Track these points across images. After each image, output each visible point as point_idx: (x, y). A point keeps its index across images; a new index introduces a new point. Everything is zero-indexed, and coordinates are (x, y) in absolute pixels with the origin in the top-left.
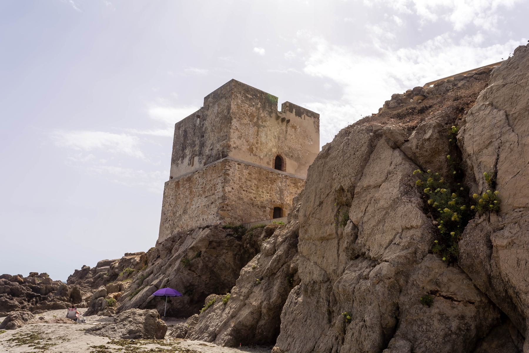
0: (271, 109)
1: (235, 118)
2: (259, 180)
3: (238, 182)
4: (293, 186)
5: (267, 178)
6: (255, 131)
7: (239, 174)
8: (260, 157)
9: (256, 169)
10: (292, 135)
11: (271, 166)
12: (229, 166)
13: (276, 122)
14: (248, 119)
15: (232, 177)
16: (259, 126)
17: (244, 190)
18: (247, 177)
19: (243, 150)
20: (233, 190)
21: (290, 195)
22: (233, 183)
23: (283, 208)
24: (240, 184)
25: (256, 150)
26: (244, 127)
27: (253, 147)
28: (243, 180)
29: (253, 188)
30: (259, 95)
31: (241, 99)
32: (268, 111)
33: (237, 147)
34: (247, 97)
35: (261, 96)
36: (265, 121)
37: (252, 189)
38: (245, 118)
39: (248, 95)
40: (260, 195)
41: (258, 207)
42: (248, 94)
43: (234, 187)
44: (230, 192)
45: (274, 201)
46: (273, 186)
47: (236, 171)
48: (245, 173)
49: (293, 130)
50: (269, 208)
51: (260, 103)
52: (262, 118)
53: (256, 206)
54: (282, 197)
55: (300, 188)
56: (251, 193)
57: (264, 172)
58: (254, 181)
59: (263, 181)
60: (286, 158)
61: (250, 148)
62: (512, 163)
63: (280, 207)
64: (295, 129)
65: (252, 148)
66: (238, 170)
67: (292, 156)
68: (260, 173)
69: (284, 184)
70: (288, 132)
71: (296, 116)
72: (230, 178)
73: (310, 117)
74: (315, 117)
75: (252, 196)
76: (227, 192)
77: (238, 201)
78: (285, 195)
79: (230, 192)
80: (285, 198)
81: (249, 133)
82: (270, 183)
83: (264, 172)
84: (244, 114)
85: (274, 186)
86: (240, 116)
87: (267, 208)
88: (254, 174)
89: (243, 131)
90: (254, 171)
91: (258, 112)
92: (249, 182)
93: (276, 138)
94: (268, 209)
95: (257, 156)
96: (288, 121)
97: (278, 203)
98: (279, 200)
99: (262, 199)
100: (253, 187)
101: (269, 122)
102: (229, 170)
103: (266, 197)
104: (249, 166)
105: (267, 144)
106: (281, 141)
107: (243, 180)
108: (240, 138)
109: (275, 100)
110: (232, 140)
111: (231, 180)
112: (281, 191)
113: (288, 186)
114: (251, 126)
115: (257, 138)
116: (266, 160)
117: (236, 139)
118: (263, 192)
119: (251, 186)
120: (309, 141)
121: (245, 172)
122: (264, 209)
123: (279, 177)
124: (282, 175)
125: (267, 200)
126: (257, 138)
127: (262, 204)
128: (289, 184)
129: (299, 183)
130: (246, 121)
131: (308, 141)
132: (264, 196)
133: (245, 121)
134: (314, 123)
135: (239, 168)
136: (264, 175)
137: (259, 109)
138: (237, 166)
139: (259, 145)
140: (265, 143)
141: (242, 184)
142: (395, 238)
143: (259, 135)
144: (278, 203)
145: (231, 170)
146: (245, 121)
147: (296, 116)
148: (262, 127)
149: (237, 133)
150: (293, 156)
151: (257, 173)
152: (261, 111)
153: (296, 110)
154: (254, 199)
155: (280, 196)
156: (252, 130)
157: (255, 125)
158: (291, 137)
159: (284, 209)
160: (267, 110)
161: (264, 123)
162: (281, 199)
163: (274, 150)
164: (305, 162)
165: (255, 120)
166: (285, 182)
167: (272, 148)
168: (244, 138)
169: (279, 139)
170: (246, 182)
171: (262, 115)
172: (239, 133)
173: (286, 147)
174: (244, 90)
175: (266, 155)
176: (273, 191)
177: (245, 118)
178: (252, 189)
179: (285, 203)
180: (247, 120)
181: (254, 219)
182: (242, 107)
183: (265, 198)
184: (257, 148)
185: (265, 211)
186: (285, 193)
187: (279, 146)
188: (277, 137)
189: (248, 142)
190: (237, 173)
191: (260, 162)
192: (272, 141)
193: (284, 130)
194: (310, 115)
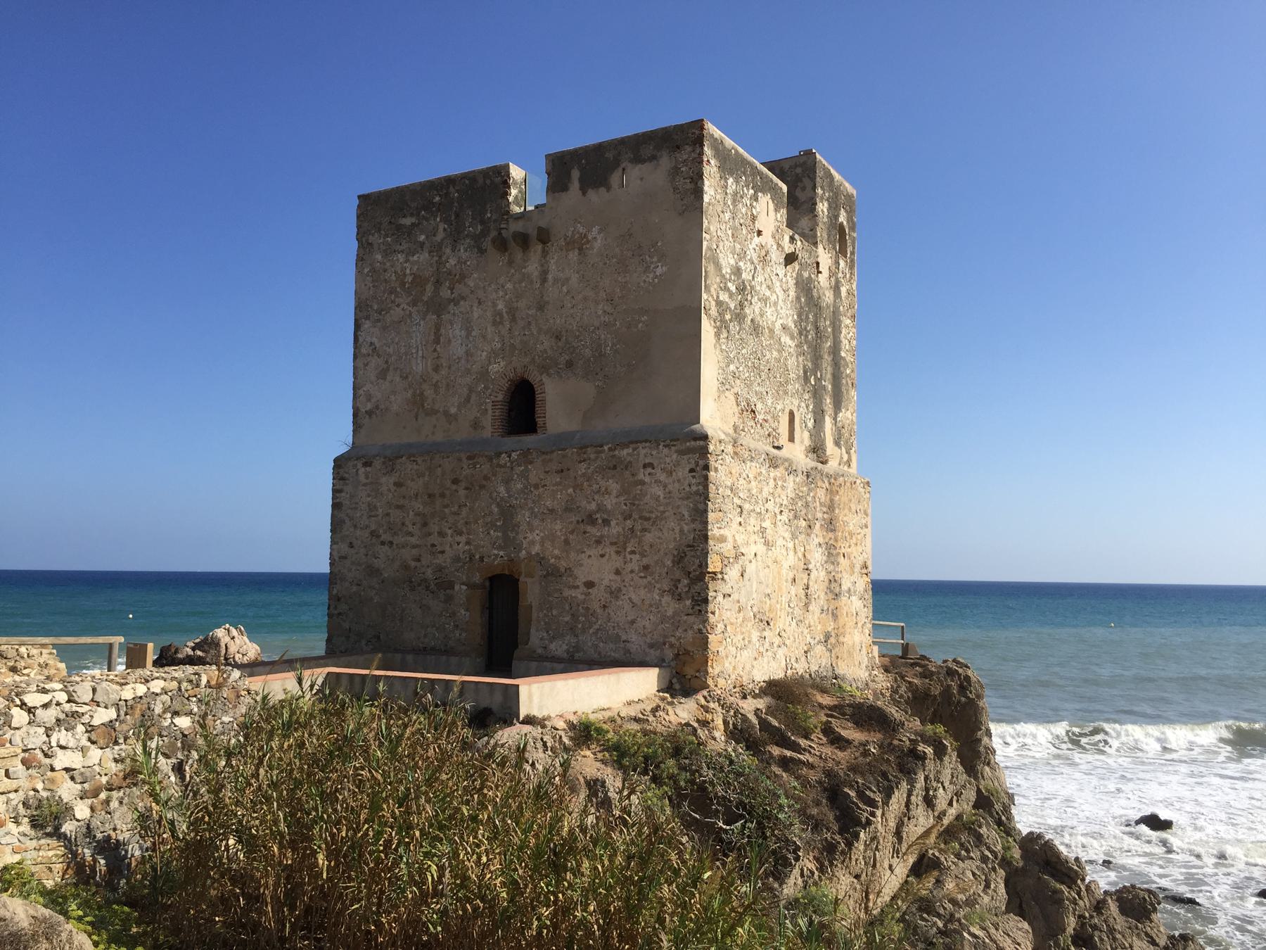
0: (482, 222)
1: (367, 318)
4: (557, 484)
8: (446, 413)
10: (568, 280)
11: (489, 426)
12: (343, 479)
15: (349, 511)
17: (383, 543)
20: (353, 551)
22: (352, 529)
23: (520, 574)
27: (425, 386)
28: (380, 510)
29: (411, 529)
30: (437, 199)
31: (383, 247)
33: (377, 407)
40: (433, 545)
41: (427, 588)
42: (404, 216)
44: (345, 558)
45: (482, 559)
47: (360, 488)
48: (384, 488)
50: (463, 584)
51: (442, 226)
52: (450, 273)
54: (511, 535)
56: (403, 547)
60: (545, 378)
61: (414, 395)
64: (580, 249)
66: (365, 485)
67: (570, 364)
69: (519, 486)
70: (550, 277)
71: (584, 193)
73: (653, 158)
76: (337, 559)
78: (524, 527)
81: (410, 347)
87: (457, 587)
89: (391, 350)
91: (436, 258)
94: (460, 589)
97: (494, 560)
98: (500, 548)
99: (439, 560)
100: (410, 526)
104: (397, 458)
107: (380, 510)
108: (382, 374)
111: (347, 521)
117: (372, 383)
119: (403, 524)
121: (387, 482)
124: (509, 456)
125: (457, 559)
126: (435, 350)
129: (583, 466)
130: (398, 310)
132: (447, 548)
133: (397, 313)
134: (675, 171)
138: (362, 470)
143: (442, 340)
144: (497, 557)
147: (584, 193)
149: (374, 361)
152: (448, 251)
154: (413, 564)
159: (522, 579)
161: (459, 288)
167: (490, 363)
168: (396, 369)
169: (513, 320)
171: (452, 262)
175: (468, 400)
180: (402, 306)
181: (412, 630)
184: (436, 386)
185: (449, 599)
186: (523, 517)
189: (407, 377)
192: (489, 336)
194: (647, 151)
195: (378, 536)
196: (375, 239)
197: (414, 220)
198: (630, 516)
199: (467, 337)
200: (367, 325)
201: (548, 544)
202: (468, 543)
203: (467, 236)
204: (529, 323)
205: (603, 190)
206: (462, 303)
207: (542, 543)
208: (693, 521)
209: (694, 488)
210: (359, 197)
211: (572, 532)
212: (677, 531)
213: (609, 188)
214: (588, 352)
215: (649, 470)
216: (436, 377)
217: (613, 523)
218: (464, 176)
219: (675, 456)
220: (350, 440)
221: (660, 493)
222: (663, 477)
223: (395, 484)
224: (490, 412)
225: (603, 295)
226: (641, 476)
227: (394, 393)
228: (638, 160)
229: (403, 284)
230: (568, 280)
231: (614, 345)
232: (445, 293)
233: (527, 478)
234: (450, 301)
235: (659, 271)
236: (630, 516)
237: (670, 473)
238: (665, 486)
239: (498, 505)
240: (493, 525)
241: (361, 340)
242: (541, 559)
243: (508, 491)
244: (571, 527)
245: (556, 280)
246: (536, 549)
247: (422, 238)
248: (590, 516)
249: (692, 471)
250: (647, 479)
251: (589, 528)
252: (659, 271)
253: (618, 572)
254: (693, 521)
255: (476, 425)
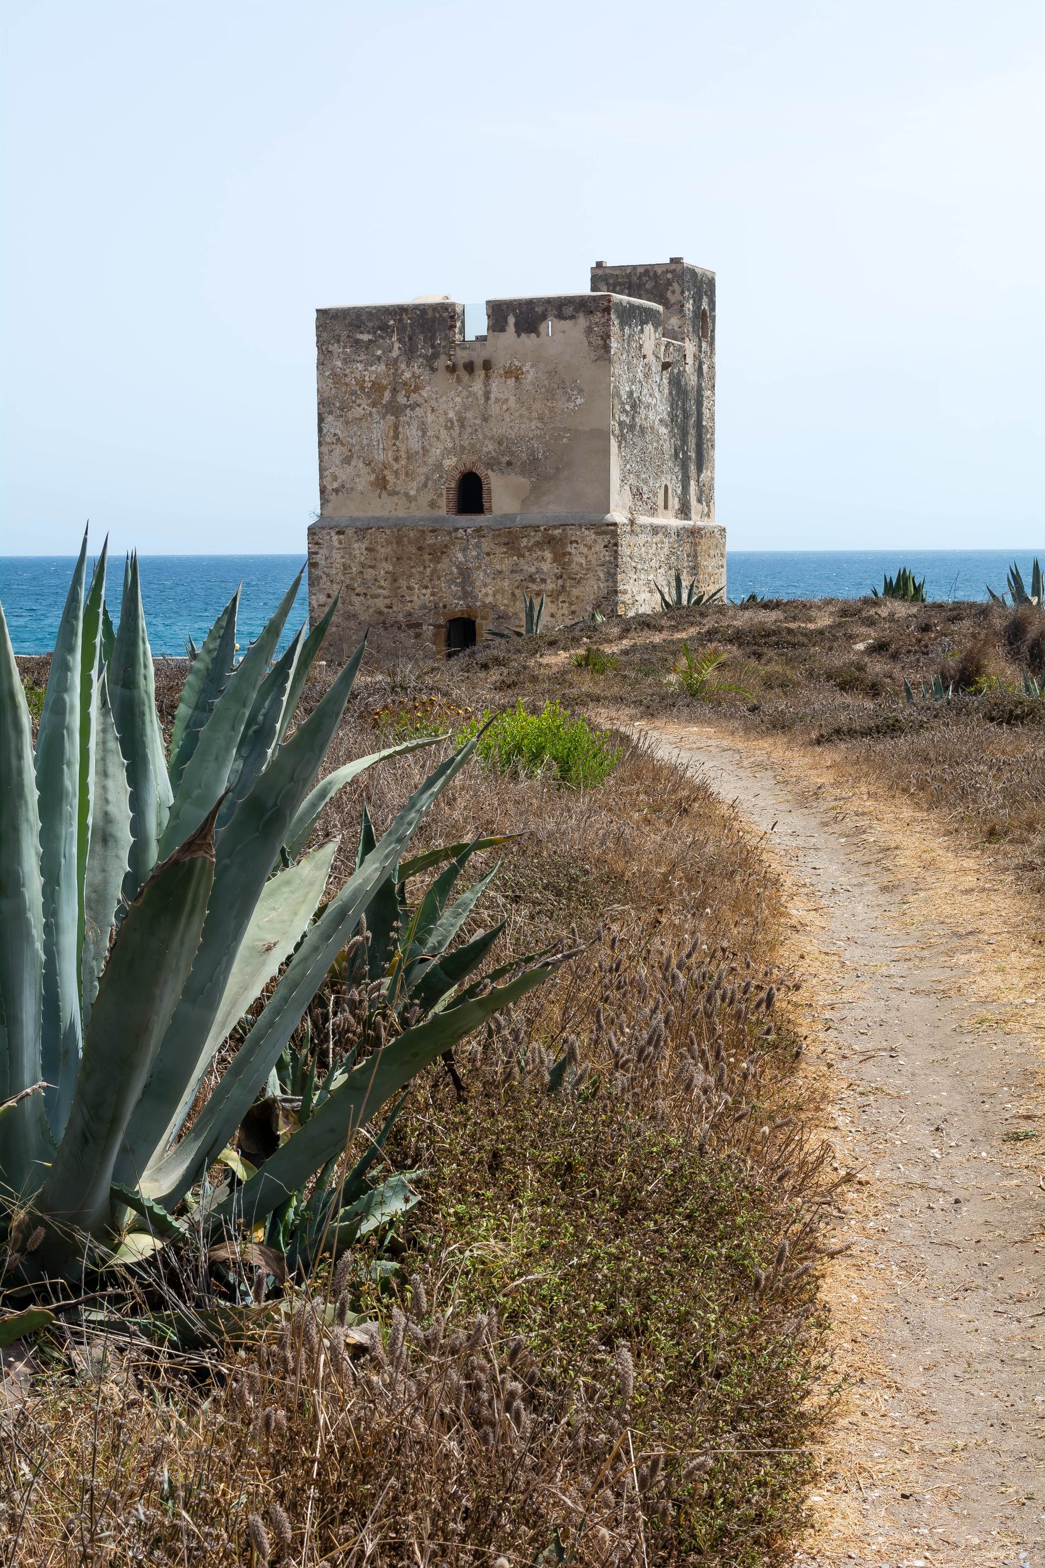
0: (433, 347)
1: (330, 413)
2: (398, 559)
3: (340, 577)
5: (420, 549)
6: (387, 429)
7: (343, 557)
8: (407, 495)
9: (388, 532)
10: (507, 400)
11: (443, 509)
12: (317, 543)
13: (452, 380)
14: (364, 402)
16: (394, 409)
17: (358, 595)
18: (363, 558)
19: (360, 488)
21: (494, 579)
23: (476, 617)
24: (348, 582)
25: (396, 477)
26: (356, 429)
27: (386, 472)
29: (382, 583)
30: (392, 322)
32: (425, 357)
33: (343, 486)
34: (357, 342)
35: (401, 320)
36: (417, 389)
37: (381, 587)
38: (358, 401)
39: (360, 337)
40: (403, 596)
41: (399, 628)
42: (361, 333)
43: (331, 592)
46: (439, 566)
48: (357, 552)
49: (511, 382)
50: (430, 625)
51: (397, 345)
52: (405, 384)
53: (392, 626)
54: (469, 589)
55: (527, 554)
57: (412, 534)
58: (384, 564)
59: (410, 559)
61: (377, 478)
62: (426, 401)
63: (466, 616)
64: (517, 378)
65: (384, 477)
66: (339, 549)
67: (509, 464)
68: (399, 542)
69: (474, 553)
70: (492, 396)
71: (519, 336)
72: (320, 573)
73: (572, 317)
74: (591, 312)
75: (380, 603)
77: (345, 624)
79: (324, 605)
80: (476, 591)
82: (431, 561)
83: (412, 534)
84: (353, 393)
85: (444, 565)
86: (343, 402)
87: (425, 627)
88: (382, 546)
90: (382, 538)
91: (392, 371)
92: (370, 570)
93: (452, 428)
95: (397, 493)
96: (487, 365)
98: (459, 599)
101: (428, 388)
102: (316, 553)
103: (420, 598)
105: (428, 451)
106: (469, 430)
108: (347, 460)
109: (445, 315)
110: (327, 473)
111: (324, 576)
112: (465, 574)
113: (488, 554)
114: (376, 417)
115: (394, 444)
116: (429, 496)
118: (409, 588)
119: (376, 580)
120: (569, 400)
121: (359, 548)
122: (417, 630)
123: (457, 538)
125: (424, 607)
126: (394, 444)
127: (409, 618)
128: (488, 550)
129: (525, 540)
131: (564, 399)
132: (415, 598)
133: (358, 412)
134: (589, 330)
135: (340, 543)
136: (409, 542)
137: (396, 360)
138: (335, 538)
139: (403, 462)
140: (421, 451)
141: (352, 579)
142: (838, 731)
143: (401, 437)
144: (458, 606)
145: (321, 551)
146: (358, 412)
147: (519, 336)
148: (408, 411)
149: (338, 449)
150: (514, 461)
151: (391, 543)
152: (403, 366)
153: (516, 317)
154: (386, 610)
155: (463, 588)
156: (379, 429)
157: (387, 412)
158: (505, 407)
159: (478, 621)
160: (420, 356)
161: (414, 397)
162: (466, 595)
163: (449, 462)
164: (557, 469)
165: (387, 395)
166: (477, 546)
168: (359, 457)
169: (462, 426)
170: (361, 572)
171: (407, 375)
172: (344, 449)
173: (487, 442)
174: (350, 325)
175: (425, 485)
176: (439, 579)
177: (358, 401)
178: (381, 587)
179: (478, 604)
182: (346, 375)
183: (417, 603)
184: (396, 473)
185: (418, 636)
187: (463, 447)
188: (456, 423)
189: (369, 464)
190: (337, 556)
191: (409, 508)
192: (442, 437)
193: (480, 393)
194: (569, 311)
195: (353, 589)
196: (335, 348)
197: (370, 337)
198: (561, 577)
199: (423, 436)
200: (330, 418)
201: (499, 596)
202: (433, 594)
203: (420, 356)
204: (476, 430)
205: (533, 335)
206: (417, 409)
207: (494, 595)
208: (607, 581)
209: (607, 558)
210: (317, 311)
211: (517, 588)
212: (595, 587)
213: (538, 336)
214: (524, 456)
215: (575, 545)
216: (396, 466)
217: (549, 581)
218: (416, 307)
219: (593, 536)
220: (318, 511)
221: (583, 561)
222: (585, 550)
223: (366, 549)
224: (445, 496)
225: (535, 415)
226: (569, 549)
227: (359, 476)
228: (561, 316)
229: (362, 388)
230: (507, 400)
231: (544, 452)
232: (402, 400)
233: (480, 548)
234: (406, 406)
235: (578, 402)
236: (561, 577)
237: (590, 548)
238: (586, 557)
239: (457, 567)
240: (453, 581)
241: (325, 431)
242: (493, 607)
243: (465, 556)
244: (516, 584)
245: (497, 400)
246: (489, 600)
247: (379, 352)
248: (531, 576)
249: (605, 546)
250: (573, 551)
251: (530, 585)
252: (578, 402)
253: (552, 616)
254: (607, 581)
255: (433, 505)
